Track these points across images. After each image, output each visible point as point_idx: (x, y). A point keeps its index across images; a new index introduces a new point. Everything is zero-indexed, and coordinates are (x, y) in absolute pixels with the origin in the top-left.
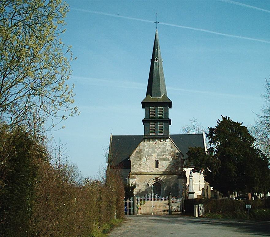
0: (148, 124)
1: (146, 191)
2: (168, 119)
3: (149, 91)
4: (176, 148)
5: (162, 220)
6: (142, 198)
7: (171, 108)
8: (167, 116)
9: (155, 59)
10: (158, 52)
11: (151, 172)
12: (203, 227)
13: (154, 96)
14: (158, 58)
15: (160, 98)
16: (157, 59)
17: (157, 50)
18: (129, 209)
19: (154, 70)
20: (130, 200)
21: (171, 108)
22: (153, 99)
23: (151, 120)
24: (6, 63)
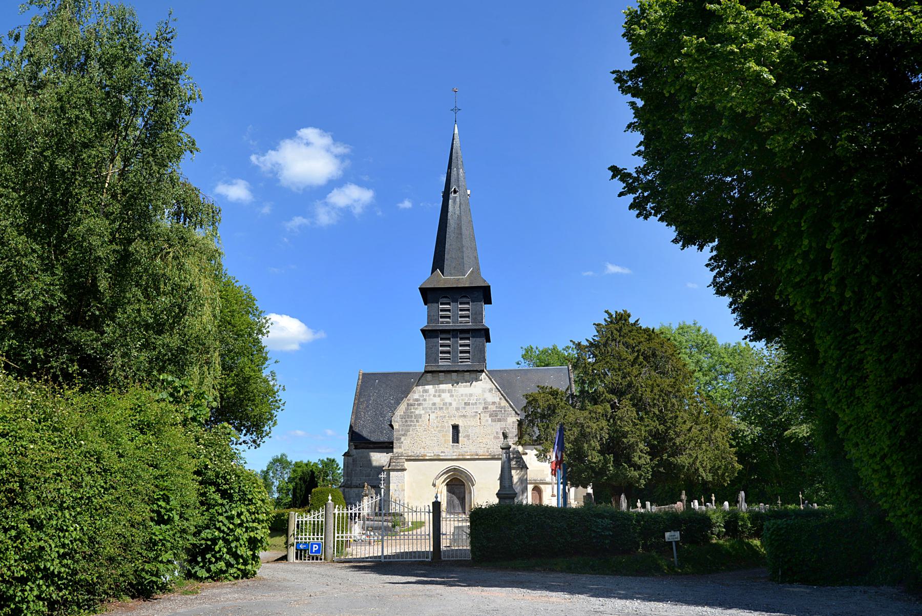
0: (435, 340)
1: (588, 509)
2: (480, 327)
3: (439, 262)
4: (502, 395)
5: (360, 562)
6: (351, 509)
7: (490, 303)
8: (479, 318)
9: (453, 190)
10: (458, 174)
11: (442, 452)
12: (315, 569)
13: (451, 275)
14: (458, 187)
15: (464, 280)
16: (457, 189)
17: (458, 169)
18: (338, 541)
19: (449, 214)
20: (316, 515)
21: (490, 303)
22: (447, 280)
23: (441, 328)
24: (874, 380)
